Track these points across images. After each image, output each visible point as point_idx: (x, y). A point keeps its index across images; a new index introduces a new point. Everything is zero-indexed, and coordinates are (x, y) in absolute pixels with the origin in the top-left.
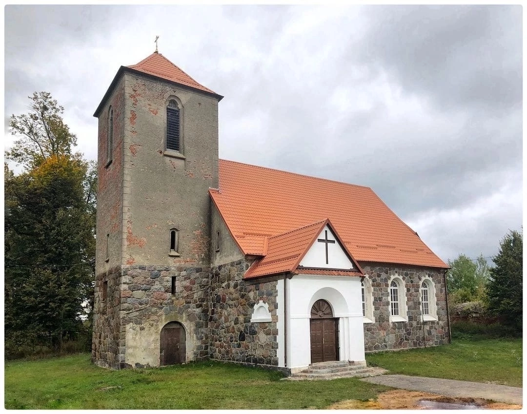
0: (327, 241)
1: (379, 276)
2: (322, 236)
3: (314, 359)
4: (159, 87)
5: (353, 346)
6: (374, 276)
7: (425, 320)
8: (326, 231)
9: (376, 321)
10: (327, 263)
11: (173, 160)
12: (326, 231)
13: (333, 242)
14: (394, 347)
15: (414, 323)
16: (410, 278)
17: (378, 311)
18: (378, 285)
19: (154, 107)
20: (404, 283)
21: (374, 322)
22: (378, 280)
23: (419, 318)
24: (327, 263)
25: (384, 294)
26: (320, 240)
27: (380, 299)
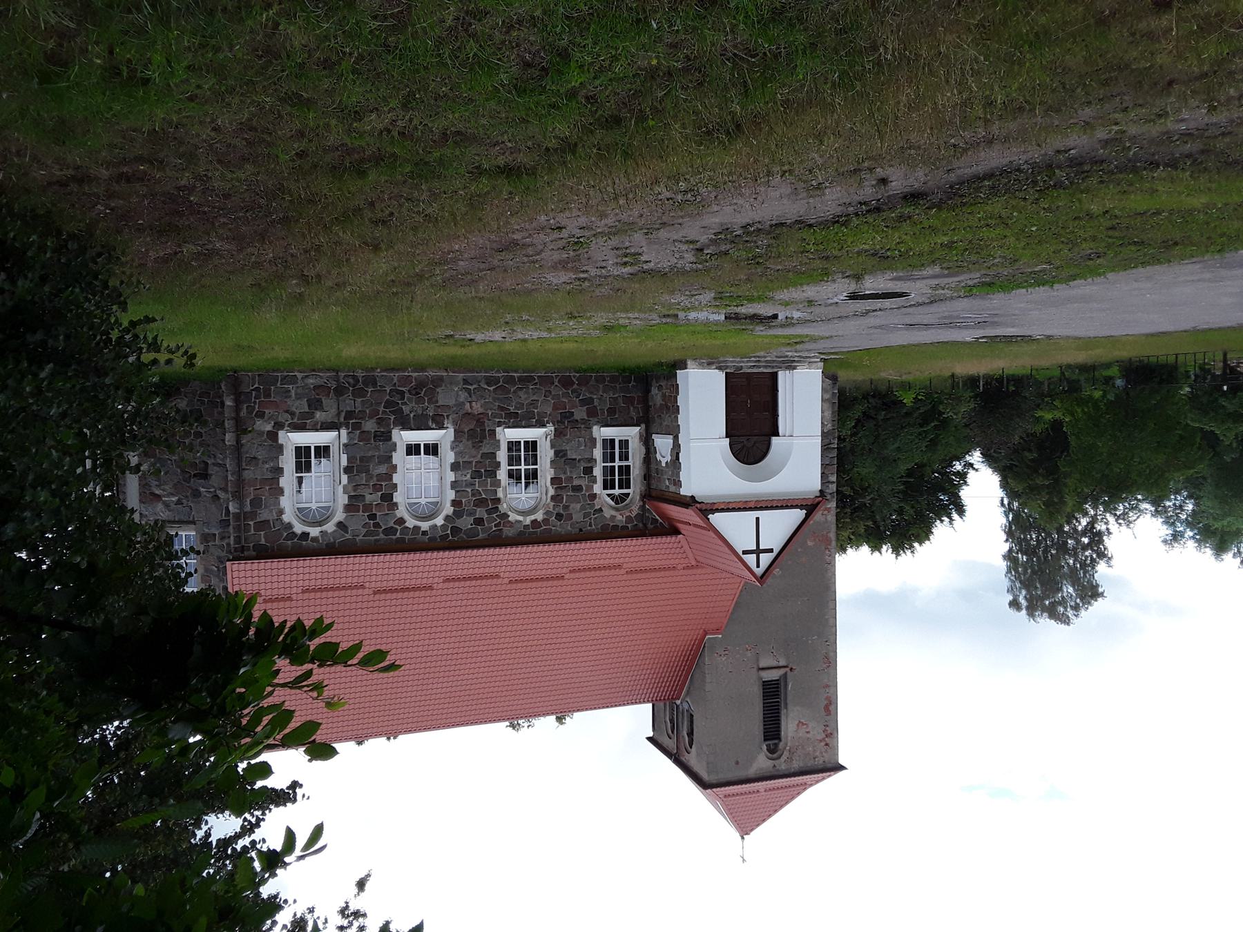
0: (758, 551)
1: (479, 521)
2: (766, 559)
3: (774, 377)
4: (796, 765)
5: (702, 396)
6: (491, 520)
7: (334, 434)
8: (758, 566)
9: (493, 433)
10: (758, 519)
11: (775, 664)
12: (758, 566)
13: (745, 552)
14: (441, 379)
15: (370, 426)
16: (377, 525)
17: (485, 450)
18: (481, 502)
19: (802, 733)
20: (286, 518)
21: (498, 430)
22: (481, 512)
23: (350, 438)
24: (758, 519)
25: (467, 486)
26: (771, 551)
27: (477, 474)
